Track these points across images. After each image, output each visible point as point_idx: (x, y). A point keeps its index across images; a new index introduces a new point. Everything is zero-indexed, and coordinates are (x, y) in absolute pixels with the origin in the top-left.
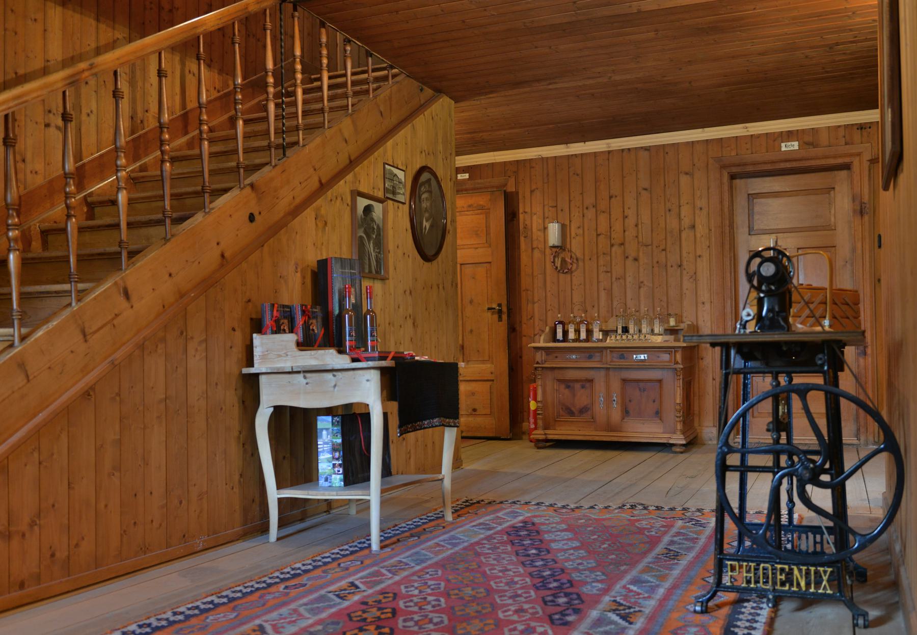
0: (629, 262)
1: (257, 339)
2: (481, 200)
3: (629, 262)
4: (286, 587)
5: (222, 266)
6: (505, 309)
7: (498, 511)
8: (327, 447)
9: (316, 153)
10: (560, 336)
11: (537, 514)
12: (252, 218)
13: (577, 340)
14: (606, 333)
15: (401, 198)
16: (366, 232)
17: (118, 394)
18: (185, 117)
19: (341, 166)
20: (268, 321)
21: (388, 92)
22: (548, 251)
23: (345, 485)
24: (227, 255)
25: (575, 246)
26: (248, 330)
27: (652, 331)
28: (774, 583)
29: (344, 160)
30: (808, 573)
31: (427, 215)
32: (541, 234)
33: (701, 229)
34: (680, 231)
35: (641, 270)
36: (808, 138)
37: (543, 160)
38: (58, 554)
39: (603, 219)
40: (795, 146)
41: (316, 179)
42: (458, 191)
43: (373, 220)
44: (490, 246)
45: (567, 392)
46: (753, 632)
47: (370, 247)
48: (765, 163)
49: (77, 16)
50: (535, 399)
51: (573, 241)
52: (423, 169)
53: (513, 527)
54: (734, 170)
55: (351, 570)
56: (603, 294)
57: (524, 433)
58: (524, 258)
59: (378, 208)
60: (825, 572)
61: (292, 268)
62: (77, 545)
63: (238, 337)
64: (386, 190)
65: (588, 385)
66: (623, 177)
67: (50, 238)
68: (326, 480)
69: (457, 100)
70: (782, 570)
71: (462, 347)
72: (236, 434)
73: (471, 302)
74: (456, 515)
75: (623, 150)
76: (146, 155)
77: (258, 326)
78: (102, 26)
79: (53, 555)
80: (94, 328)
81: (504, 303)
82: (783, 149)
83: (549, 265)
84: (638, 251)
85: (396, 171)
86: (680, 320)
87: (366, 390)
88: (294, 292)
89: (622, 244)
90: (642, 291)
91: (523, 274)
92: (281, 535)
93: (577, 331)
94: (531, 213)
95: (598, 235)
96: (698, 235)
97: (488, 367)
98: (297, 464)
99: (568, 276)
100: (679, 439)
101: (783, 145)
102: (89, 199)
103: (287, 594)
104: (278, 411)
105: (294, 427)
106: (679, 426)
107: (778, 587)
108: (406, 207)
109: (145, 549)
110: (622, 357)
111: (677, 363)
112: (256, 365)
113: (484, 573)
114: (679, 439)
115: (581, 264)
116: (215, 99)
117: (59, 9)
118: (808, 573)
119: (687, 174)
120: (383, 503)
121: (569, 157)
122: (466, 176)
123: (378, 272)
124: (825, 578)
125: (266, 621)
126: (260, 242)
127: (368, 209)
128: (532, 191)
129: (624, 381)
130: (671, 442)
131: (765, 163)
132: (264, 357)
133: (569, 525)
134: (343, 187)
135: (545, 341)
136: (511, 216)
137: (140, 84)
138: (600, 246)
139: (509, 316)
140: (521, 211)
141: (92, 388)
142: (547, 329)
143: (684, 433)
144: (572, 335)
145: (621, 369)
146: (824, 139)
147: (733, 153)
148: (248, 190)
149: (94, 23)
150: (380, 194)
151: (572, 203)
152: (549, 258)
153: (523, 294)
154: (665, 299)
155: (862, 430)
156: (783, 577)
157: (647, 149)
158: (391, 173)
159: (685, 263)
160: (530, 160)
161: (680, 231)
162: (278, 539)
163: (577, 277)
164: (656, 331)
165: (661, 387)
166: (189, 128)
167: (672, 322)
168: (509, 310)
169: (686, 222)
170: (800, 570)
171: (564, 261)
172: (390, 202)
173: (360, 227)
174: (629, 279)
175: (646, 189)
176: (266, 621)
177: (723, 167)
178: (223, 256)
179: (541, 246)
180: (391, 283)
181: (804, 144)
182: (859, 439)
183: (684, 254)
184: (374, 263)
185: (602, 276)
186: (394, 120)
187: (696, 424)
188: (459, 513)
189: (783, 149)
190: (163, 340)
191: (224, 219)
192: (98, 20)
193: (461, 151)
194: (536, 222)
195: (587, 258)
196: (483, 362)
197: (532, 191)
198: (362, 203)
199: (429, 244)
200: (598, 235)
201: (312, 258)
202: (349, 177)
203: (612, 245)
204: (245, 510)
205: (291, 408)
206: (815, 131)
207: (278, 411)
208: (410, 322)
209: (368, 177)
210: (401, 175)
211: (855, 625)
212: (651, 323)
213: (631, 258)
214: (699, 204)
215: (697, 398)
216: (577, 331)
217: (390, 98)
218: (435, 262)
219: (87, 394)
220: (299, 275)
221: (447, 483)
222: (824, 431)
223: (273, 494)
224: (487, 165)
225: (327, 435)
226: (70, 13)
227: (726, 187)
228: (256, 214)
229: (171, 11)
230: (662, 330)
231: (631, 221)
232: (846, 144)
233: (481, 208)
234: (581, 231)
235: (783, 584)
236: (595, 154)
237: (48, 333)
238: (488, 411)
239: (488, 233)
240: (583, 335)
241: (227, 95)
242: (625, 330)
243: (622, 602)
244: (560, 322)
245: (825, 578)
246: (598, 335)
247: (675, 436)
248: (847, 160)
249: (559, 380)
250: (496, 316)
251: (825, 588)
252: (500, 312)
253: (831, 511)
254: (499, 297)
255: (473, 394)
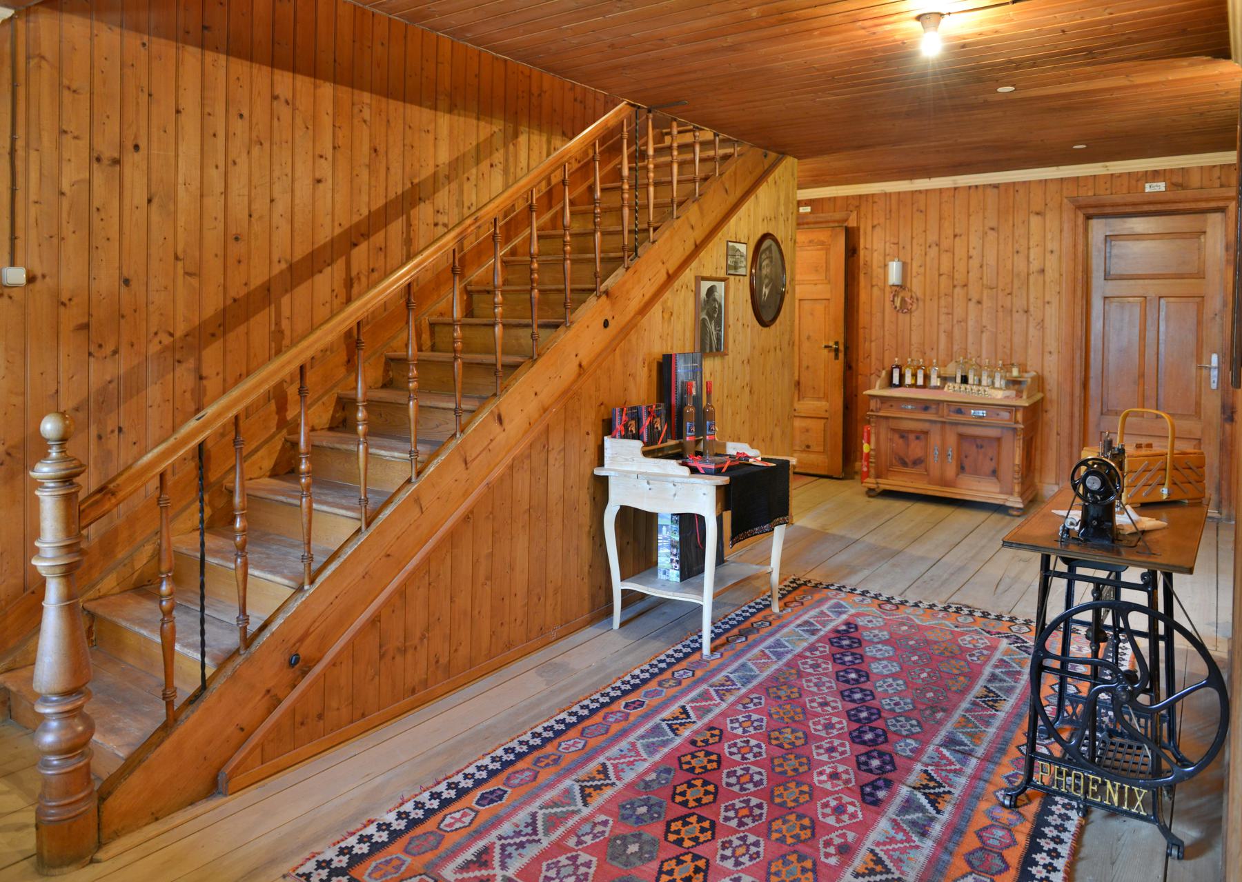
0: (972, 305)
1: (608, 441)
2: (823, 236)
3: (972, 305)
4: (626, 706)
5: (580, 375)
6: (842, 348)
7: (821, 602)
8: (667, 543)
9: (667, 247)
10: (896, 380)
11: (861, 610)
12: (606, 324)
13: (914, 385)
14: (944, 379)
15: (742, 271)
16: (708, 314)
17: (492, 513)
18: (550, 193)
19: (687, 253)
20: (618, 425)
21: (733, 168)
22: (888, 289)
23: (682, 580)
24: (584, 364)
25: (916, 286)
26: (600, 432)
27: (993, 383)
28: (1086, 792)
29: (690, 247)
30: (1122, 788)
31: (766, 281)
32: (881, 271)
33: (1051, 274)
34: (1028, 274)
35: (985, 314)
36: (1177, 180)
37: (887, 195)
38: (441, 661)
39: (946, 258)
40: (1161, 186)
41: (663, 273)
42: (799, 224)
43: (715, 300)
44: (829, 282)
45: (901, 441)
46: (1052, 876)
47: (712, 327)
48: (1126, 205)
49: (462, 119)
50: (869, 442)
51: (914, 280)
52: (766, 236)
53: (836, 631)
54: (1091, 211)
55: (685, 684)
56: (943, 337)
57: (856, 473)
58: (863, 296)
59: (720, 286)
60: (1140, 792)
61: (640, 364)
62: (456, 650)
63: (591, 442)
64: (728, 267)
65: (922, 436)
66: (969, 215)
67: (437, 329)
68: (665, 573)
69: (799, 158)
70: (1095, 782)
71: (798, 383)
72: (587, 529)
73: (809, 338)
74: (782, 603)
75: (970, 187)
76: (516, 235)
77: (608, 428)
78: (482, 124)
79: (437, 662)
80: (474, 456)
81: (841, 341)
82: (1147, 190)
83: (888, 305)
84: (982, 293)
85: (738, 246)
86: (1023, 369)
87: (700, 496)
88: (641, 390)
89: (965, 285)
90: (985, 336)
91: (861, 311)
92: (626, 618)
93: (914, 375)
94: (873, 244)
95: (940, 275)
96: (1048, 280)
97: (824, 404)
98: (639, 555)
99: (908, 316)
100: (1015, 502)
101: (1147, 185)
102: (469, 288)
103: (627, 716)
104: (624, 511)
105: (638, 526)
106: (1017, 488)
107: (1089, 797)
108: (747, 279)
109: (509, 646)
110: (959, 411)
111: (1016, 422)
112: (606, 466)
113: (804, 707)
114: (1015, 502)
115: (921, 303)
116: (577, 170)
117: (447, 116)
118: (1122, 788)
119: (1038, 214)
120: (715, 606)
121: (913, 193)
122: (808, 209)
123: (718, 350)
124: (1139, 799)
125: (609, 759)
126: (611, 348)
127: (711, 291)
128: (873, 227)
129: (961, 437)
130: (1008, 504)
131: (1126, 205)
132: (613, 459)
133: (891, 634)
134: (688, 275)
135: (882, 388)
136: (852, 251)
137: (512, 170)
138: (942, 286)
139: (846, 354)
140: (862, 246)
141: (472, 512)
142: (884, 373)
143: (1022, 495)
144: (908, 380)
145: (957, 424)
146: (1195, 180)
147: (1091, 193)
148: (604, 297)
149: (475, 122)
150: (722, 274)
151: (915, 241)
152: (889, 297)
153: (861, 331)
154: (1008, 345)
155: (1224, 503)
156: (1095, 788)
157: (996, 186)
158: (734, 248)
159: (1031, 309)
160: (873, 195)
161: (1028, 274)
162: (622, 625)
163: (916, 318)
164: (997, 384)
165: (999, 446)
166: (554, 202)
167: (1015, 372)
168: (846, 348)
169: (1035, 266)
170: (1114, 786)
171: (903, 300)
172: (732, 278)
173: (703, 309)
174: (971, 323)
175: (992, 229)
176: (609, 759)
177: (1079, 208)
178: (580, 366)
179: (881, 284)
180: (729, 358)
181: (1173, 186)
182: (1220, 513)
183: (1032, 300)
184: (715, 342)
185: (943, 318)
186: (739, 193)
187: (1037, 480)
188: (787, 599)
189: (1147, 190)
190: (530, 456)
191: (584, 335)
192: (478, 119)
193: (801, 186)
194: (877, 258)
195: (928, 298)
196: (819, 399)
197: (873, 227)
198: (705, 285)
199: (766, 310)
200: (940, 275)
201: (658, 349)
202: (694, 264)
203: (954, 286)
204: (593, 597)
205: (636, 509)
206: (1184, 171)
207: (624, 511)
208: (747, 390)
209: (712, 260)
210: (742, 248)
211: (1168, 855)
212: (992, 377)
213: (974, 300)
214: (1049, 246)
215: (1038, 452)
216: (914, 375)
217: (735, 173)
218: (773, 327)
219: (466, 518)
220: (646, 369)
221: (775, 577)
222: (1147, 661)
223: (618, 586)
224: (829, 199)
225: (667, 536)
226: (456, 118)
227: (1080, 230)
228: (610, 319)
229: (540, 95)
230: (1003, 382)
231: (975, 263)
232: (1222, 186)
233: (822, 243)
234: (922, 270)
235: (1095, 794)
236: (941, 191)
237: (437, 468)
238: (821, 449)
239: (827, 269)
240: (920, 381)
241: (587, 164)
242: (965, 380)
243: (933, 774)
244: (897, 367)
245: (1139, 799)
246: (935, 381)
247: (1012, 499)
248: (1221, 204)
249: (894, 430)
250: (833, 354)
251: (1139, 807)
252: (837, 350)
253: (1176, 632)
254: (836, 335)
255: (807, 431)
